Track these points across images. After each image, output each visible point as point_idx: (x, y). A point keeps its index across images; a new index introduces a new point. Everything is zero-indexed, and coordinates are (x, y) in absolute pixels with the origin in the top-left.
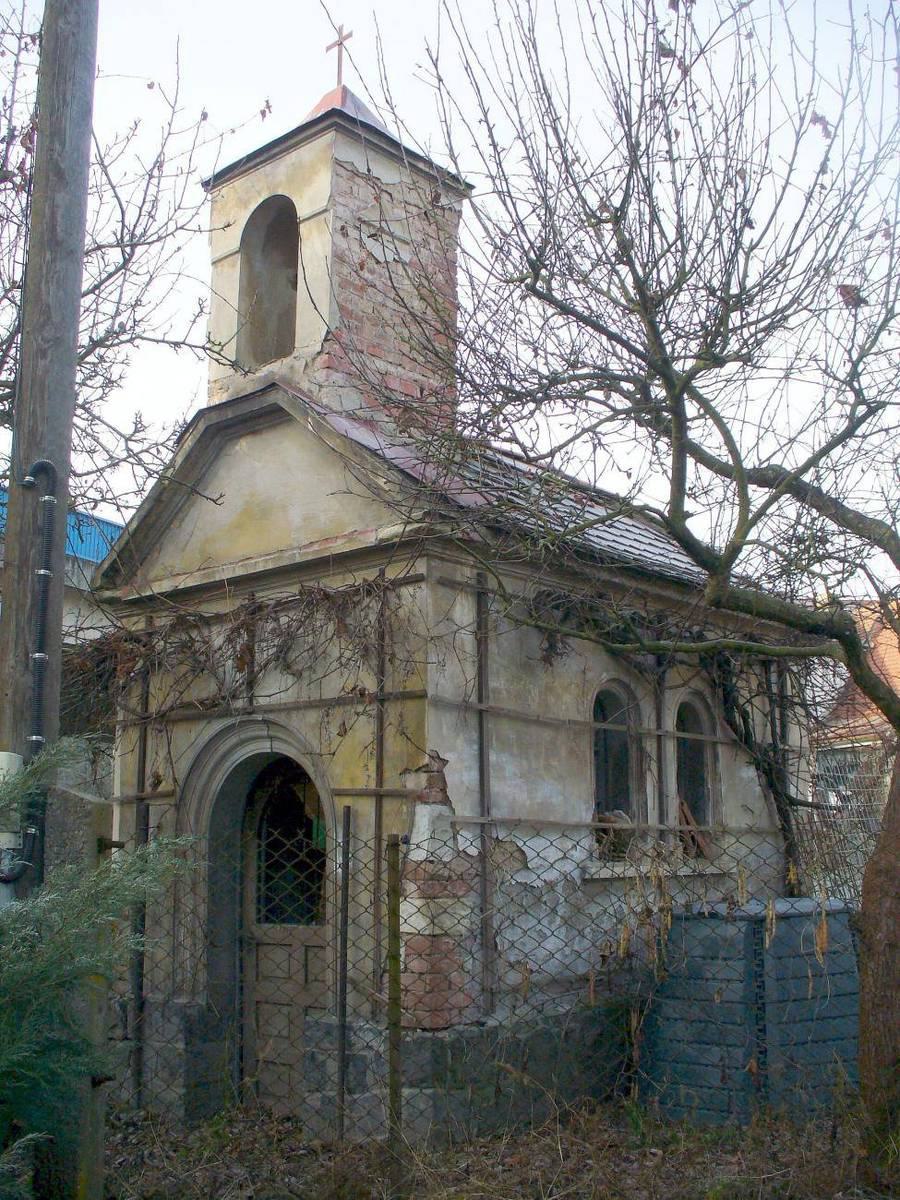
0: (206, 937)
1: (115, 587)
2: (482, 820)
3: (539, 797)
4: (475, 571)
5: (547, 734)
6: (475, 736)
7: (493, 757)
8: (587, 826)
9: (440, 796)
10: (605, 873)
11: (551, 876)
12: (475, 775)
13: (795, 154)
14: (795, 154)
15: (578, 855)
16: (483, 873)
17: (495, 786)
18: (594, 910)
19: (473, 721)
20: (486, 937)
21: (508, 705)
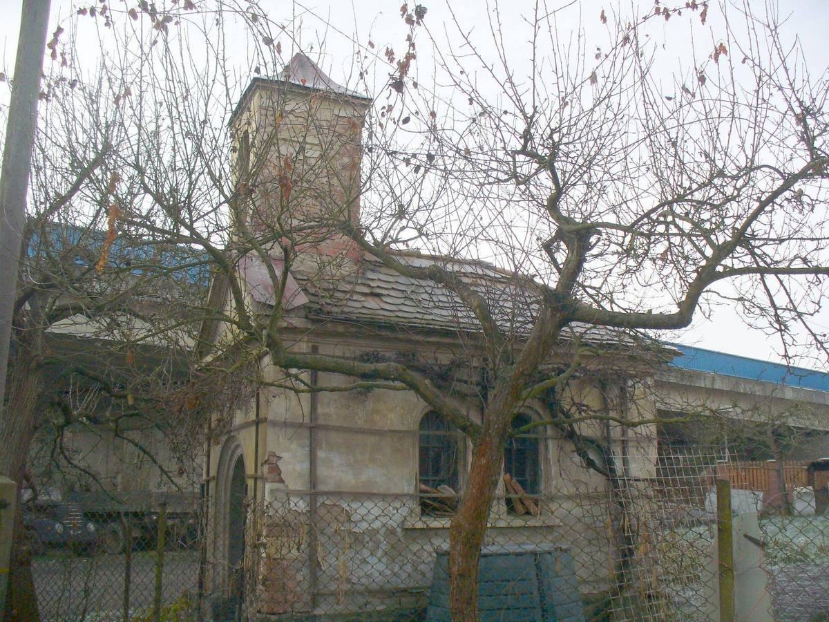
0: (777, 434)
1: (262, 339)
2: (622, 439)
3: (364, 478)
4: (310, 344)
5: (372, 439)
6: (307, 442)
7: (321, 454)
8: (411, 496)
9: (277, 478)
10: (419, 525)
11: (377, 525)
12: (306, 465)
13: (534, 55)
14: (534, 55)
15: (404, 511)
16: (313, 524)
17: (322, 471)
18: (415, 548)
19: (306, 433)
20: (314, 564)
21: (334, 422)
